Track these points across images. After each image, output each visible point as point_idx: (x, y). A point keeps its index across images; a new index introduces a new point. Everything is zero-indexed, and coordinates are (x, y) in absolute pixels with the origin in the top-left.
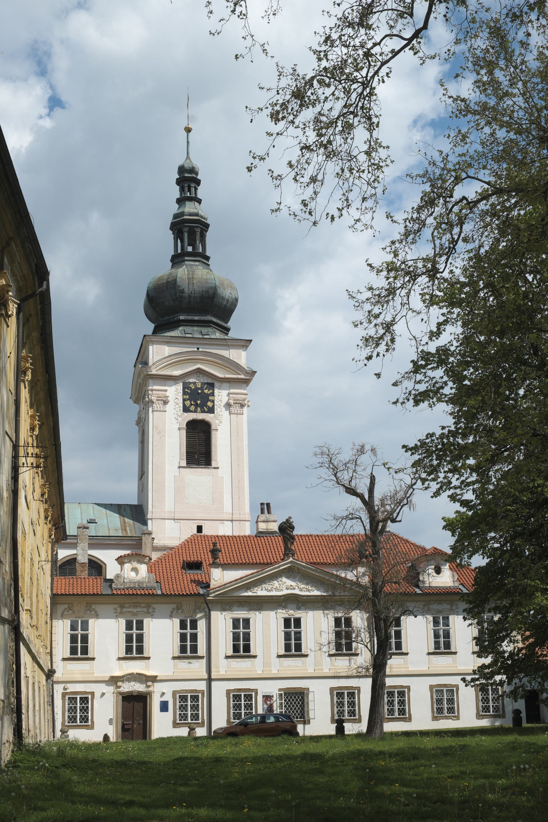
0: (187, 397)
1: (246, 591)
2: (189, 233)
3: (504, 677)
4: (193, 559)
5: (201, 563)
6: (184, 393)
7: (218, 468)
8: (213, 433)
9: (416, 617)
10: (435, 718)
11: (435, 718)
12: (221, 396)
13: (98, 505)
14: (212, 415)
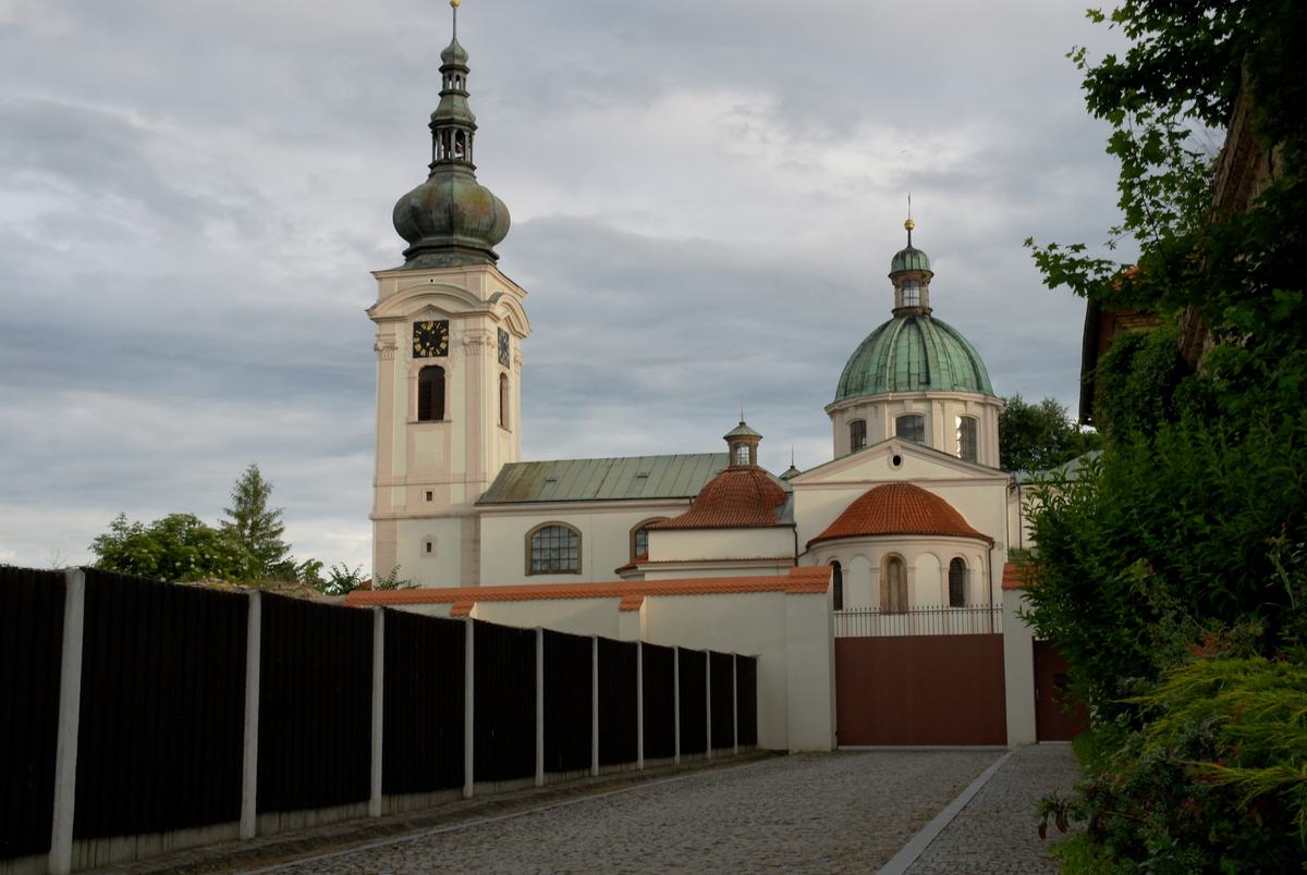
0: (418, 340)
2: (451, 131)
6: (415, 336)
9: (893, 312)
10: (531, 572)
11: (531, 572)
12: (457, 330)
14: (443, 359)
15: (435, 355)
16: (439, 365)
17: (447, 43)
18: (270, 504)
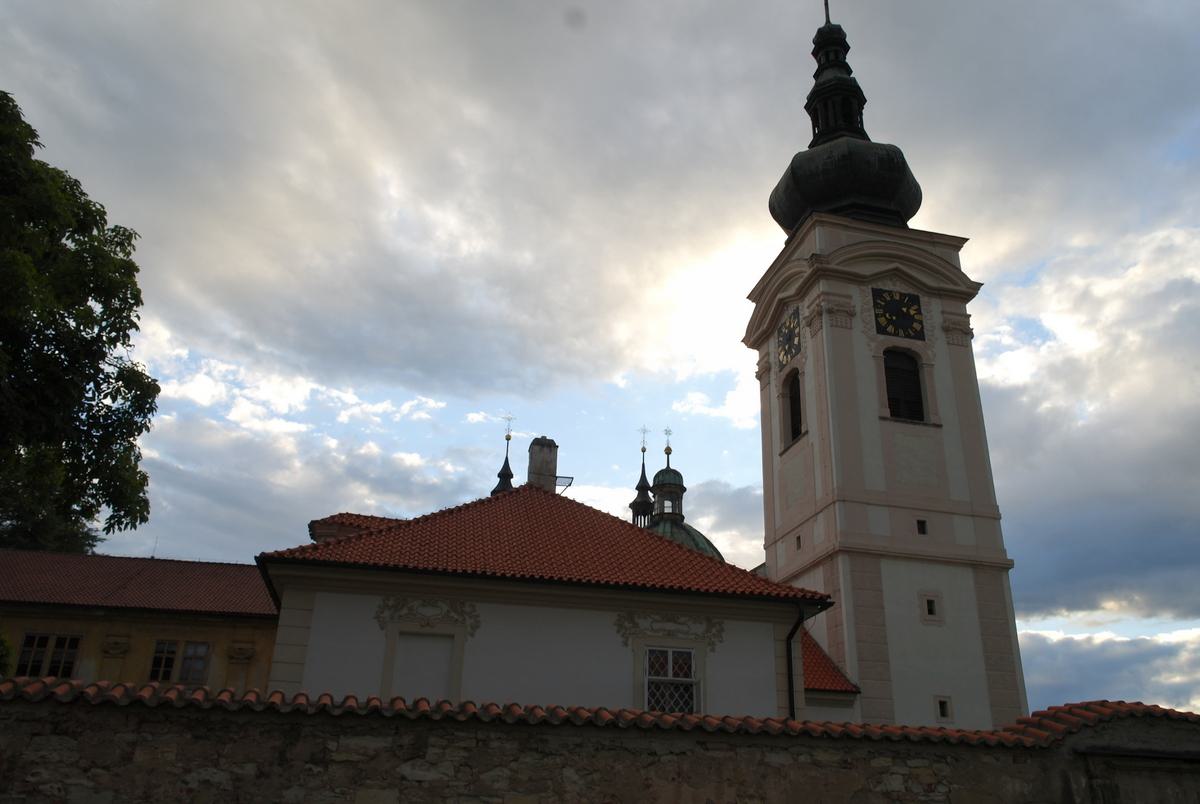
3: (64, 241)
4: (937, 608)
6: (876, 305)
7: (940, 426)
8: (925, 375)
13: (507, 458)
14: (919, 342)
15: (908, 336)
17: (822, 23)
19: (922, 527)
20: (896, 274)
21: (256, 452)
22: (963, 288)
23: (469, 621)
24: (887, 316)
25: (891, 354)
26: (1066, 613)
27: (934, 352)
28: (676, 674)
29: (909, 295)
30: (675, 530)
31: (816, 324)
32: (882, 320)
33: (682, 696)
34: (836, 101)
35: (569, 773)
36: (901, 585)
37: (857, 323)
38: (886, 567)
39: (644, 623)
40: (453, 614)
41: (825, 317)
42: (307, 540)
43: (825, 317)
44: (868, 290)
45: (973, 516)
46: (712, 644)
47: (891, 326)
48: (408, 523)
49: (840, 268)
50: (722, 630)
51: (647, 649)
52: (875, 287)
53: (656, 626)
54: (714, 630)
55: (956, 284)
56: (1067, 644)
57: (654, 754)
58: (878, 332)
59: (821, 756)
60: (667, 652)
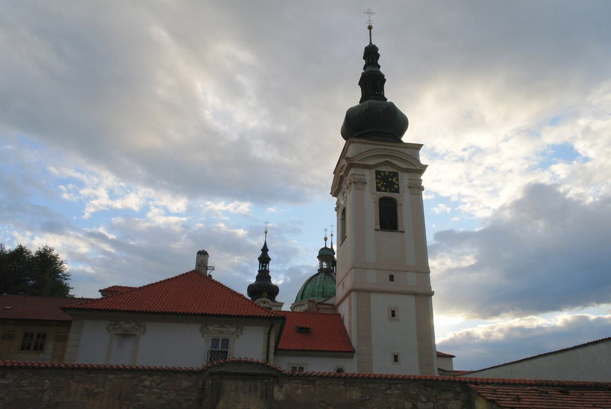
1: (110, 252)
4: (396, 314)
5: (390, 276)
6: (377, 178)
7: (403, 232)
14: (396, 194)
15: (391, 191)
16: (393, 197)
17: (367, 44)
18: (269, 253)
19: (392, 278)
20: (387, 163)
21: (163, 234)
22: (418, 168)
23: (142, 329)
24: (382, 183)
25: (382, 201)
26: (596, 305)
27: (404, 199)
28: (222, 348)
29: (376, 175)
30: (327, 277)
31: (350, 189)
32: (379, 185)
33: (224, 356)
34: (372, 82)
35: (47, 381)
36: (379, 305)
37: (367, 187)
38: (373, 297)
39: (211, 328)
40: (136, 327)
41: (353, 185)
42: (99, 296)
43: (353, 185)
44: (373, 171)
45: (416, 272)
46: (238, 336)
47: (383, 188)
48: (136, 289)
49: (359, 162)
50: (243, 330)
51: (211, 338)
52: (377, 170)
53: (216, 329)
54: (239, 330)
55: (416, 166)
56: (599, 320)
57: (73, 375)
58: (377, 191)
59: (125, 375)
60: (219, 339)
